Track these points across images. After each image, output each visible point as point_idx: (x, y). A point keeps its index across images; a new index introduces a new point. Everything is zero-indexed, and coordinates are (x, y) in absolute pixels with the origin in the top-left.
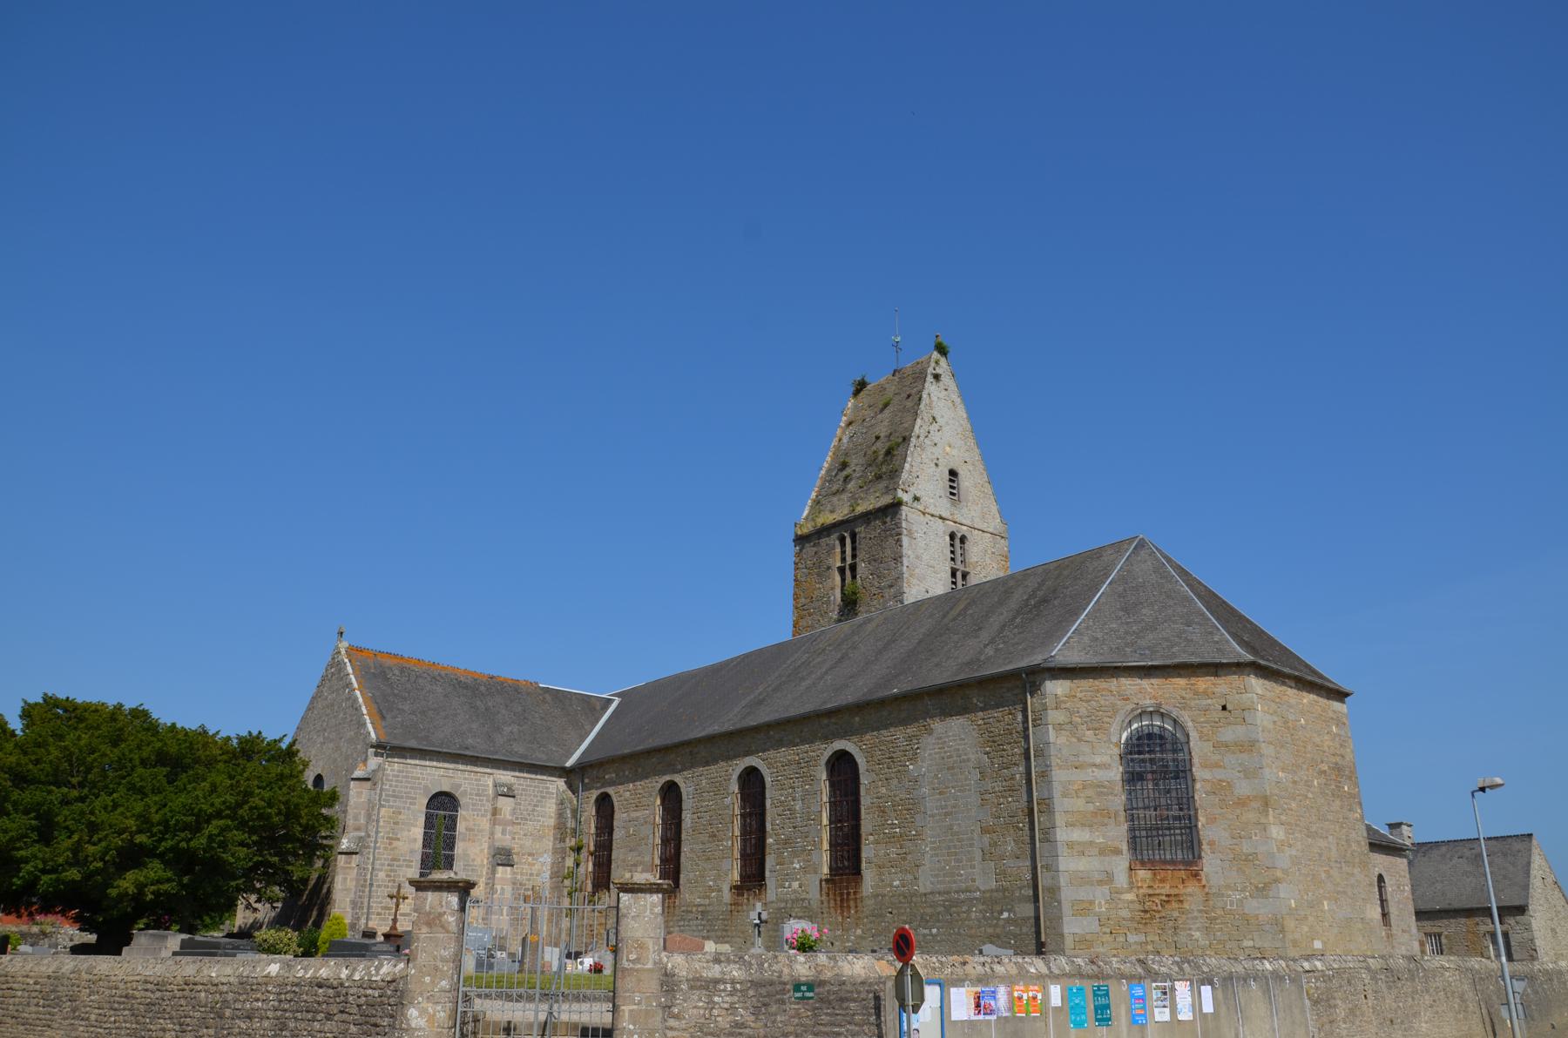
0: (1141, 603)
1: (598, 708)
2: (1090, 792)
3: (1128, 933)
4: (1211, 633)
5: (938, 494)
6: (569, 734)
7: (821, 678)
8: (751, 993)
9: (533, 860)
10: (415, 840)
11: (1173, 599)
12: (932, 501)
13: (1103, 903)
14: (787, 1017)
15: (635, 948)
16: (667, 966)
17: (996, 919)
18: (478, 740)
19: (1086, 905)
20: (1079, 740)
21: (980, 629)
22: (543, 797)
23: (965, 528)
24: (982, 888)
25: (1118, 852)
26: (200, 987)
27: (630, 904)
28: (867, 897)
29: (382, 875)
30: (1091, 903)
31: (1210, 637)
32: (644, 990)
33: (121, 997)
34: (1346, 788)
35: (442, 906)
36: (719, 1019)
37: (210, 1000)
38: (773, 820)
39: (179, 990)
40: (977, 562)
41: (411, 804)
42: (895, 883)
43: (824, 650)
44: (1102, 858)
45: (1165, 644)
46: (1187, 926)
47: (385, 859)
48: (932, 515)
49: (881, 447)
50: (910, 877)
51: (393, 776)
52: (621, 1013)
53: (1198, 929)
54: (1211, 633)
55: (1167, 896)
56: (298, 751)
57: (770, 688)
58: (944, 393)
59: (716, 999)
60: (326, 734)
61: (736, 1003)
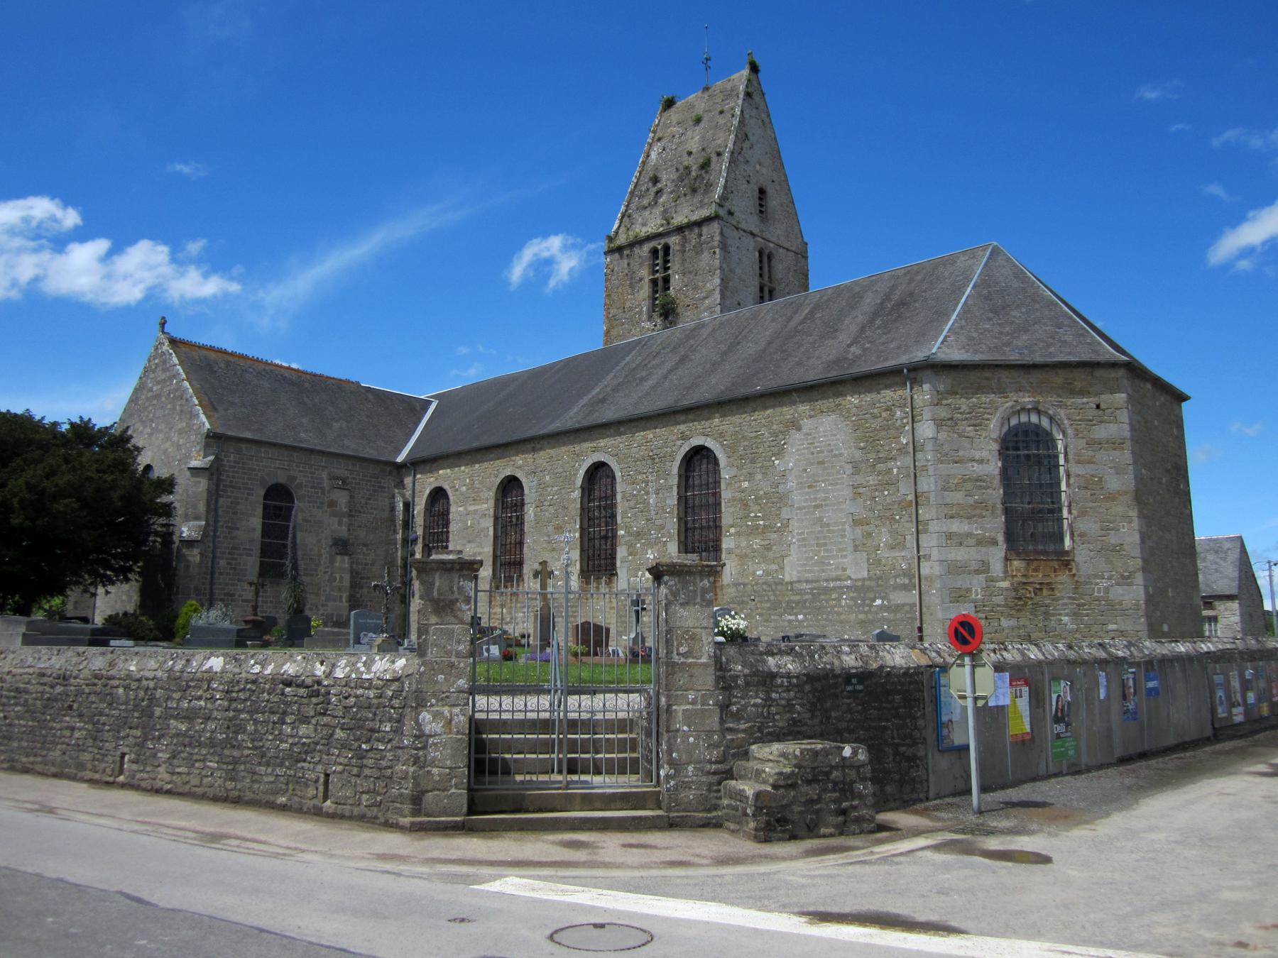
0: (1008, 306)
1: (418, 408)
2: (969, 486)
3: (1002, 618)
4: (1082, 335)
5: (749, 211)
6: (394, 432)
7: (665, 377)
8: (807, 688)
9: (367, 550)
10: (254, 530)
11: (1039, 303)
12: (744, 217)
13: (979, 590)
14: (840, 713)
15: (686, 640)
16: (721, 659)
17: (868, 605)
18: (311, 435)
19: (963, 593)
20: (960, 436)
21: (836, 331)
22: (375, 491)
23: (772, 245)
24: (853, 577)
25: (994, 542)
26: (116, 682)
27: (678, 589)
28: (728, 585)
29: (223, 563)
30: (969, 590)
31: (1082, 339)
32: (699, 688)
33: (9, 691)
34: (1182, 486)
35: (453, 593)
36: (777, 717)
37: (132, 697)
38: (625, 512)
39: (87, 685)
40: (782, 279)
41: (248, 494)
42: (758, 573)
43: (658, 353)
44: (979, 548)
45: (1041, 345)
46: (1058, 612)
47: (226, 548)
48: (744, 231)
49: (694, 163)
50: (775, 567)
51: (230, 467)
52: (674, 714)
53: (1066, 615)
54: (1082, 335)
55: (1040, 584)
56: (131, 437)
57: (608, 389)
58: (755, 111)
59: (774, 695)
60: (154, 425)
61: (793, 700)
